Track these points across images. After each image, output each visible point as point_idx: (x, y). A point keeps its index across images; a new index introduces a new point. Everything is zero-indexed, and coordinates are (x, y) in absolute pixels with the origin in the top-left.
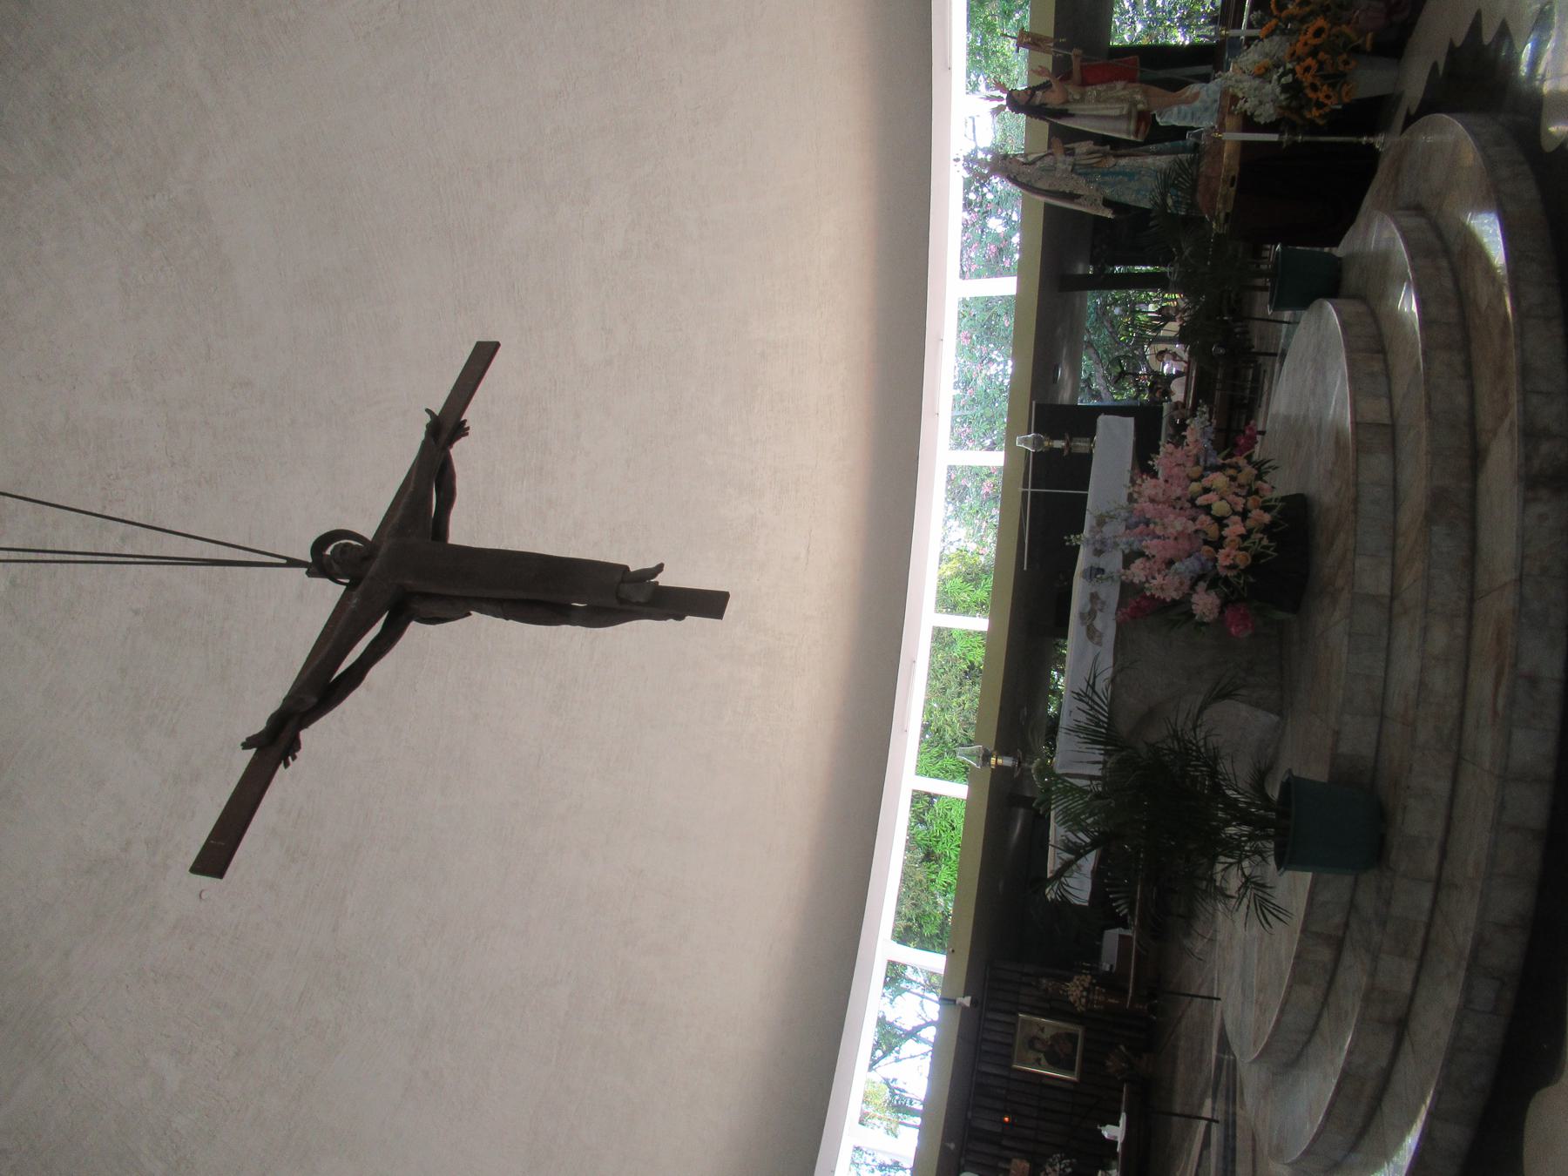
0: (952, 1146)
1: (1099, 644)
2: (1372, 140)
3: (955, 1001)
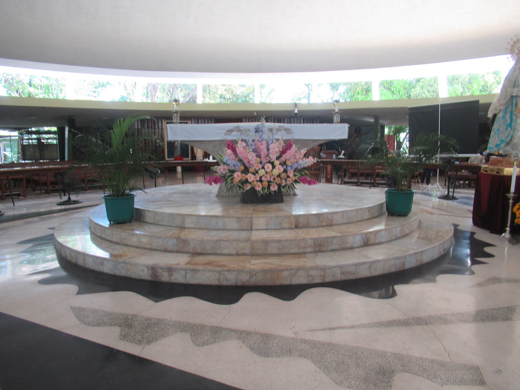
0: (255, 114)
1: (225, 134)
2: (508, 232)
3: (296, 107)
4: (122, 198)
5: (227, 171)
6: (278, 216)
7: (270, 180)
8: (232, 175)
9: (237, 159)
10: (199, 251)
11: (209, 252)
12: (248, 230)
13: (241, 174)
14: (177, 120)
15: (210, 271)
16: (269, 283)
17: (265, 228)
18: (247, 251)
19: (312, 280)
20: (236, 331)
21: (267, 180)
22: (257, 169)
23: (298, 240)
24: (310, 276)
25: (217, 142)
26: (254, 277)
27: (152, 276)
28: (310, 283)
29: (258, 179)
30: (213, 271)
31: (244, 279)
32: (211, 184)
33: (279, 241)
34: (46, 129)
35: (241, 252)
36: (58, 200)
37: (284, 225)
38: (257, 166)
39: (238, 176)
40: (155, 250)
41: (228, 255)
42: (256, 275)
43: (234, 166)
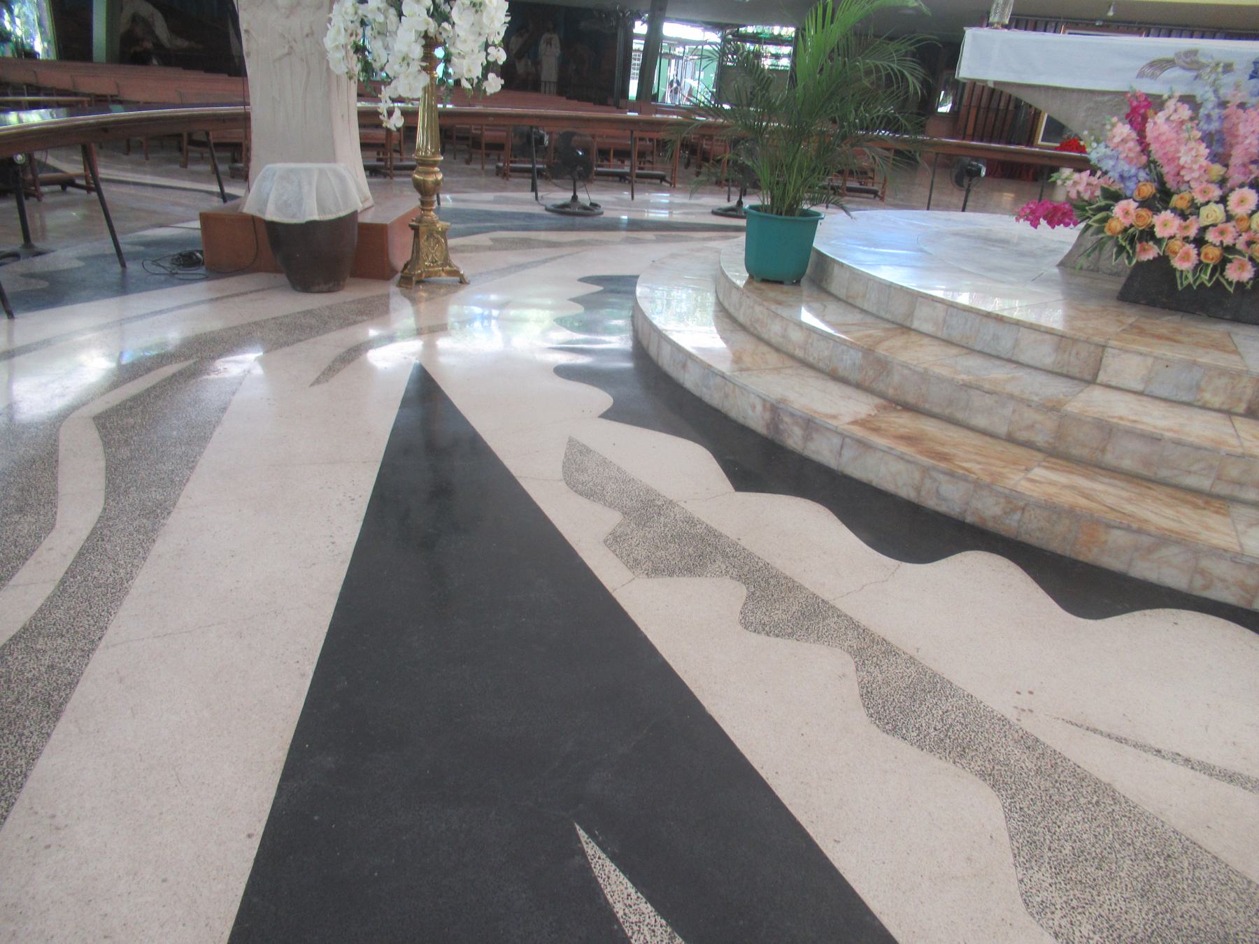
1: (1141, 75)
4: (789, 218)
5: (1098, 193)
6: (1195, 363)
7: (1234, 245)
8: (1108, 208)
9: (1144, 159)
10: (911, 399)
11: (937, 410)
12: (1081, 380)
13: (1138, 207)
14: (1002, 15)
15: (901, 458)
16: (1055, 546)
17: (1140, 387)
18: (1040, 439)
19: (1206, 587)
20: (863, 632)
21: (1222, 242)
22: (1200, 199)
23: (1223, 453)
24: (1203, 572)
25: (1106, 98)
26: (1017, 516)
27: (768, 426)
28: (1195, 593)
29: (1192, 233)
30: (908, 461)
31: (987, 509)
32: (1035, 224)
33: (1154, 439)
34: (777, 30)
35: (1023, 435)
36: (721, 202)
37: (1207, 396)
38: (1204, 192)
39: (1124, 213)
40: (811, 366)
41: (984, 433)
42: (1023, 509)
43: (1122, 178)
